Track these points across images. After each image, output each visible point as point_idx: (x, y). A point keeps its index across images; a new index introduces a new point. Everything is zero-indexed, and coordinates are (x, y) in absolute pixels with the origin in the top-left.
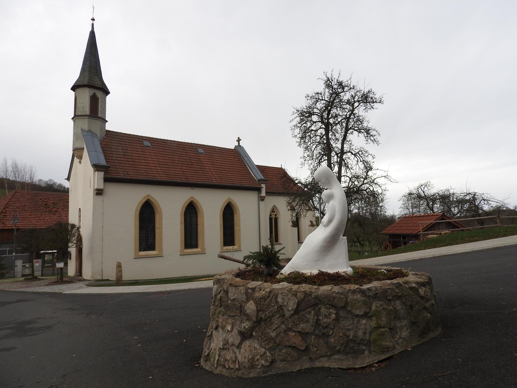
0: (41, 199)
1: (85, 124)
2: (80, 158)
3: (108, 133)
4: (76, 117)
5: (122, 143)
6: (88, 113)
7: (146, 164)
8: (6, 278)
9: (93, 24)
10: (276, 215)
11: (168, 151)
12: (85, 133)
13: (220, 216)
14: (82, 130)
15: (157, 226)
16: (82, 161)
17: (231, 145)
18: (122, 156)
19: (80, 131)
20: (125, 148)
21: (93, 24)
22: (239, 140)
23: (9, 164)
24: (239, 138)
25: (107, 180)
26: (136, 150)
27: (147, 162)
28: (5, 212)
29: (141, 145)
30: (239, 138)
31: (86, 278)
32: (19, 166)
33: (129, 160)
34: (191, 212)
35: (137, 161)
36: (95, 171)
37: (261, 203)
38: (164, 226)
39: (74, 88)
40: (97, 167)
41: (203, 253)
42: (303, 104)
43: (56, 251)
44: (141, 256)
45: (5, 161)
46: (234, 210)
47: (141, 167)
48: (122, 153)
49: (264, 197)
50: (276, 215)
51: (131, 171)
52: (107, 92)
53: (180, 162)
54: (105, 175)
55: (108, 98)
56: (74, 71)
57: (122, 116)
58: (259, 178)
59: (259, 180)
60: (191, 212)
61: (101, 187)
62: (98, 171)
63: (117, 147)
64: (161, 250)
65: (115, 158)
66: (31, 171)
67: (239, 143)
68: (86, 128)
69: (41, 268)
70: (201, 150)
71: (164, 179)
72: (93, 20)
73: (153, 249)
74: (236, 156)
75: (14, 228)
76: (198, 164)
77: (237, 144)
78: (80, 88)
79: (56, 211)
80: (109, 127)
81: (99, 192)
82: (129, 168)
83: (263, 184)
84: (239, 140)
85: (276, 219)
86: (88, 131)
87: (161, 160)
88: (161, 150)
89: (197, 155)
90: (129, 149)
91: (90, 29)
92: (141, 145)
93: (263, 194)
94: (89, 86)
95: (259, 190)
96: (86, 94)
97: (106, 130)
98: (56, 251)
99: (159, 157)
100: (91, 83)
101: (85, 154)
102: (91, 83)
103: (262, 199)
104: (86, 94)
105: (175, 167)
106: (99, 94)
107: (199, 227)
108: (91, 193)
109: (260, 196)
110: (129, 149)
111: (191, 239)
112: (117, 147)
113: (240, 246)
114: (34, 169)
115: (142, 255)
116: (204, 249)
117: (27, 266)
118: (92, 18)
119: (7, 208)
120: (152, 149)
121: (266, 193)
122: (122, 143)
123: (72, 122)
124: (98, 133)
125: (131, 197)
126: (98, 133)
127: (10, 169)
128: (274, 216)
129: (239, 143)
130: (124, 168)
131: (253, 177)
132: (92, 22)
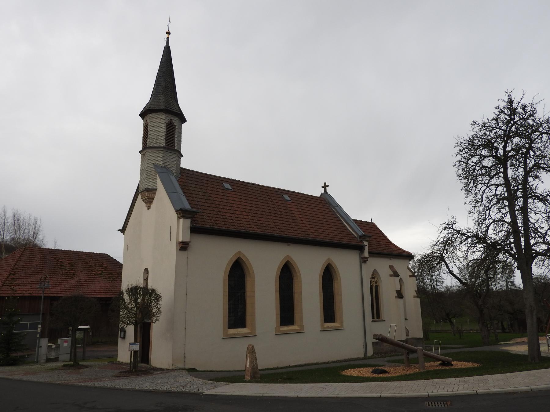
0: (55, 258)
1: (159, 158)
2: (149, 202)
3: (182, 170)
4: (146, 148)
5: (200, 184)
6: (163, 144)
7: (232, 212)
8: (29, 363)
9: (168, 38)
10: (376, 283)
11: (252, 196)
12: (159, 170)
13: (319, 282)
14: (155, 166)
15: (248, 293)
16: (152, 206)
17: (317, 192)
18: (204, 201)
19: (152, 168)
20: (205, 191)
21: (168, 38)
22: (325, 186)
23: (9, 214)
24: (325, 183)
25: (195, 230)
26: (217, 193)
27: (232, 208)
28: (14, 275)
29: (222, 188)
30: (325, 183)
31: (158, 366)
32: (22, 217)
33: (213, 205)
34: (287, 276)
35: (221, 207)
36: (179, 218)
37: (363, 265)
38: (257, 294)
39: (143, 115)
40: (182, 213)
41: (301, 332)
42: (468, 132)
43: (88, 327)
44: (230, 335)
45: (4, 210)
46: (295, 278)
47: (228, 214)
48: (202, 197)
49: (367, 258)
50: (376, 283)
51: (218, 219)
52: (183, 120)
53: (268, 211)
54: (192, 223)
55: (184, 125)
56: (144, 95)
57: (203, 151)
58: (360, 234)
59: (361, 237)
60: (287, 276)
61: (187, 239)
62: (184, 217)
63: (196, 189)
64: (253, 328)
65: (197, 203)
66: (35, 224)
67: (325, 190)
68: (161, 164)
69: (69, 350)
70: (287, 197)
71: (256, 230)
72: (168, 33)
73: (243, 325)
74: (324, 205)
75: (42, 295)
76: (288, 214)
77: (323, 190)
78: (154, 114)
79: (74, 274)
80: (185, 163)
81: (183, 246)
82: (216, 216)
83: (365, 241)
84: (325, 186)
85: (377, 287)
86: (162, 167)
87: (247, 208)
88: (244, 195)
89: (283, 202)
90: (208, 192)
91: (165, 44)
92: (222, 188)
93: (366, 254)
94: (166, 111)
95: (361, 249)
96: (160, 122)
97: (182, 168)
98: (88, 327)
99: (245, 204)
100: (164, 108)
101: (162, 195)
102: (164, 108)
103: (364, 260)
104: (160, 122)
105: (264, 216)
106: (176, 121)
107: (296, 296)
108: (173, 247)
109: (362, 256)
110: (208, 192)
111: (287, 314)
112: (196, 189)
113: (342, 323)
114: (39, 222)
115: (232, 334)
116: (302, 327)
117: (54, 347)
118: (167, 31)
119: (16, 268)
120: (234, 193)
121: (369, 253)
122: (200, 184)
123: (140, 155)
124: (174, 169)
125: (218, 255)
126: (174, 169)
127: (10, 220)
128: (374, 284)
129: (325, 190)
130: (209, 215)
131: (350, 232)
132: (167, 36)
